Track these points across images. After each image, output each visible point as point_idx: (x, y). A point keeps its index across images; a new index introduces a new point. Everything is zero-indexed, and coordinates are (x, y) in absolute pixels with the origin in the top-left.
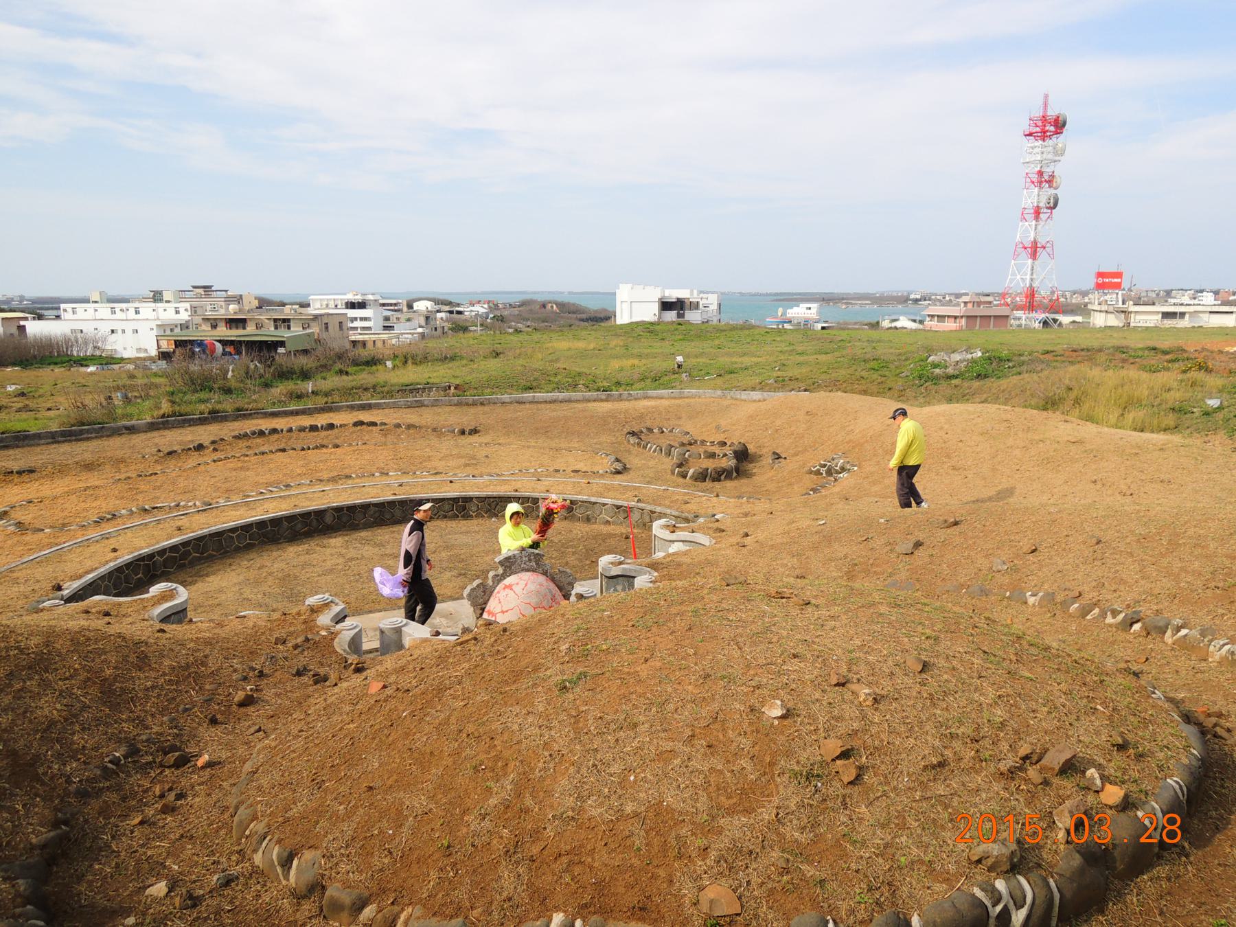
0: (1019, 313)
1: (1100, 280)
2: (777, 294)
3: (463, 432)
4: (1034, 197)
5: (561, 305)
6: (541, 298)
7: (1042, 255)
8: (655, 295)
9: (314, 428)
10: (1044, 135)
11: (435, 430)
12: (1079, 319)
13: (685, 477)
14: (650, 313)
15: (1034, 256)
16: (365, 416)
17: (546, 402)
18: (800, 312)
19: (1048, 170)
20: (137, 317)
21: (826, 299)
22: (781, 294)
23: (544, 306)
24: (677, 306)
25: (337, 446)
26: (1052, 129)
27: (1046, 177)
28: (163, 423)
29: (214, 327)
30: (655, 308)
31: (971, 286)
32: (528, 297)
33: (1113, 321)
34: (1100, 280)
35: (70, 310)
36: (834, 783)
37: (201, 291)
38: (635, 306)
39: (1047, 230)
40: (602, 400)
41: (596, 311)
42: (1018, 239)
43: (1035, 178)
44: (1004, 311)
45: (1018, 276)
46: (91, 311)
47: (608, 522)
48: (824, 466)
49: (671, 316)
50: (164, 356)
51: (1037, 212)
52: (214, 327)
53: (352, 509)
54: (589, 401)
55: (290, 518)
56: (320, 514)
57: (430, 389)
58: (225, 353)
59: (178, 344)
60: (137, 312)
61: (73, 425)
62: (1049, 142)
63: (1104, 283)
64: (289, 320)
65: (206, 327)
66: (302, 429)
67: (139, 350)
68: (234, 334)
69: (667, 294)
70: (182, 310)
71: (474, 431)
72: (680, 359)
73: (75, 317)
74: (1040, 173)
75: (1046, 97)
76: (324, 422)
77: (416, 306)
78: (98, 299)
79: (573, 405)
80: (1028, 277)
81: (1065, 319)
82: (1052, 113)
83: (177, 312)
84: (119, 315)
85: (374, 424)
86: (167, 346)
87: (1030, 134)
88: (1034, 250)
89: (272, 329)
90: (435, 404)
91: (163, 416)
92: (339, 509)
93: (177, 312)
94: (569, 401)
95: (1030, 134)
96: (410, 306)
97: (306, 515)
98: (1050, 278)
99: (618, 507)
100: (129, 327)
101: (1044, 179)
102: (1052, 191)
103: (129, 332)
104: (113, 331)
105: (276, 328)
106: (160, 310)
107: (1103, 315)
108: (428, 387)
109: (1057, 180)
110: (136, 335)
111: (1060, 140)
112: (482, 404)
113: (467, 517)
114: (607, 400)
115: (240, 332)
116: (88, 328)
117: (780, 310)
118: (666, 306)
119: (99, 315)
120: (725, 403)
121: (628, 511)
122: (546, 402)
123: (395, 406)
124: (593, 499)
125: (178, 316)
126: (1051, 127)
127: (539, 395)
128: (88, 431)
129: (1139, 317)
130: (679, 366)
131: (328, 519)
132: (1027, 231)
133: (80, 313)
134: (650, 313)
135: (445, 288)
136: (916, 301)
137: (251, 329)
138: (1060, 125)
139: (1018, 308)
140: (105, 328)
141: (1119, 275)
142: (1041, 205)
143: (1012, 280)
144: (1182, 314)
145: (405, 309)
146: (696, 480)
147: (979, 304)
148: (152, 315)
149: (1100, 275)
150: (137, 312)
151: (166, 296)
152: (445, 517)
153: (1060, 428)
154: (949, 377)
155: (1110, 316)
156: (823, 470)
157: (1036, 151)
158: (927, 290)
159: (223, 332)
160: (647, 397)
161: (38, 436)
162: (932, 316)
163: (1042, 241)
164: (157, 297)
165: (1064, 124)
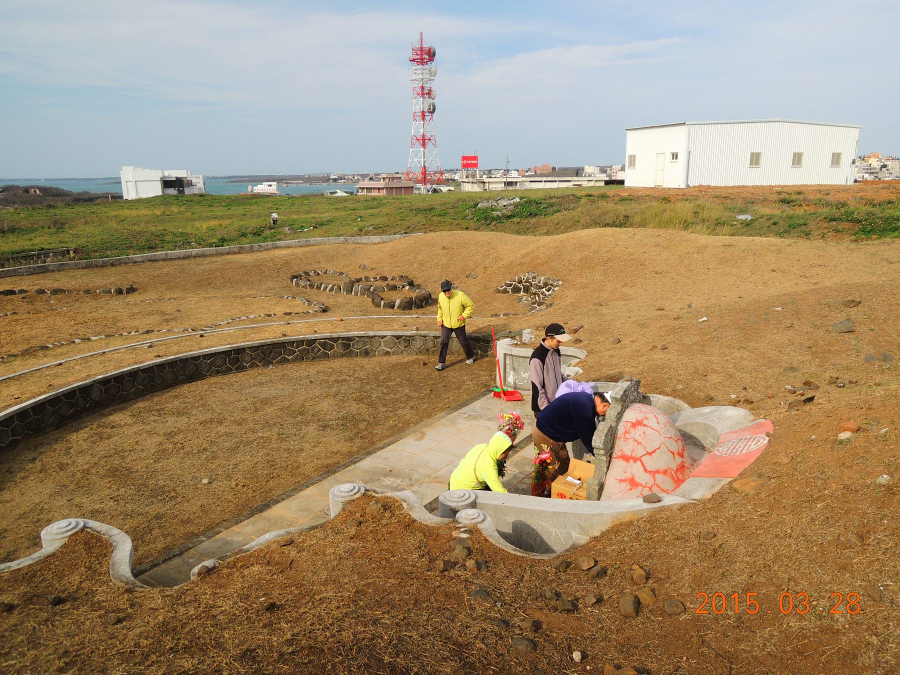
0: (419, 185)
1: (465, 162)
2: (229, 177)
3: (120, 292)
4: (420, 104)
5: (44, 190)
6: (22, 184)
7: (429, 145)
8: (157, 175)
10: (422, 62)
11: (87, 292)
12: (452, 188)
13: (393, 307)
14: (156, 190)
15: (424, 145)
17: (179, 258)
18: (262, 188)
19: (427, 86)
21: (279, 180)
22: (236, 177)
24: (178, 184)
26: (427, 57)
27: (426, 91)
31: (387, 170)
32: (10, 183)
33: (476, 188)
34: (465, 162)
38: (140, 184)
39: (431, 128)
40: (235, 253)
41: (79, 194)
43: (419, 91)
44: (411, 184)
45: (413, 161)
47: (388, 353)
48: (510, 285)
49: (172, 191)
53: (119, 379)
54: (222, 254)
55: (53, 401)
56: (84, 390)
57: (47, 255)
62: (425, 66)
69: (166, 174)
71: (131, 290)
72: (275, 215)
75: (421, 34)
79: (209, 259)
81: (444, 189)
82: (426, 46)
85: (12, 292)
87: (414, 60)
88: (424, 141)
90: (61, 268)
92: (105, 381)
94: (203, 256)
95: (414, 60)
97: (70, 395)
98: (438, 159)
99: (398, 337)
101: (426, 93)
102: (431, 101)
107: (470, 185)
108: (43, 253)
111: (433, 65)
112: (113, 265)
113: (241, 369)
114: (239, 253)
117: (250, 188)
120: (351, 247)
121: (409, 340)
124: (371, 334)
126: (425, 56)
127: (160, 253)
129: (491, 186)
130: (275, 222)
131: (95, 395)
132: (418, 128)
134: (156, 190)
136: (335, 180)
138: (431, 55)
139: (417, 182)
141: (475, 158)
143: (412, 162)
144: (516, 183)
146: (404, 309)
147: (393, 178)
149: (464, 158)
152: (218, 372)
153: (717, 237)
154: (509, 217)
155: (475, 185)
156: (509, 289)
157: (417, 73)
158: (341, 173)
160: (276, 248)
162: (363, 188)
163: (428, 135)
165: (434, 54)
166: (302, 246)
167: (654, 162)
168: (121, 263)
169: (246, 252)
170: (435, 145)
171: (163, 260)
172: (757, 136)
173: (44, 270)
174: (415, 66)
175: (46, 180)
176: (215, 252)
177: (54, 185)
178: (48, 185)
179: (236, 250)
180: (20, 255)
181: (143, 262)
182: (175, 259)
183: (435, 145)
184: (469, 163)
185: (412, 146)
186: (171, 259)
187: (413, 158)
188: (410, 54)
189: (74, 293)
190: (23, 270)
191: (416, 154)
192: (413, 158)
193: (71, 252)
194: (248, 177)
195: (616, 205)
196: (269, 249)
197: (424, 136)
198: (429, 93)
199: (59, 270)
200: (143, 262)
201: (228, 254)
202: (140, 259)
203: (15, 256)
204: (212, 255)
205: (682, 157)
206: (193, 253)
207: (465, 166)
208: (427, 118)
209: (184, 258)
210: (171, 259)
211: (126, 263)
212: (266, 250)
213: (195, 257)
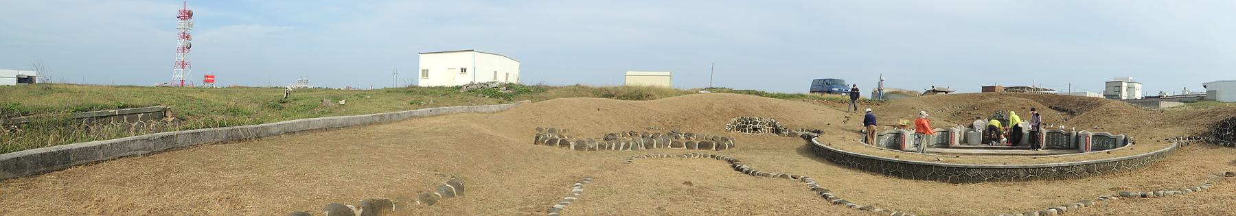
4: (181, 43)
8: (15, 73)
10: (184, 18)
40: (377, 123)
88: (183, 65)
132: (180, 57)
134: (13, 82)
138: (190, 15)
157: (182, 24)
167: (441, 71)
171: (303, 131)
172: (464, 59)
174: (180, 21)
179: (377, 119)
188: (177, 13)
190: (138, 145)
195: (416, 95)
205: (208, 85)
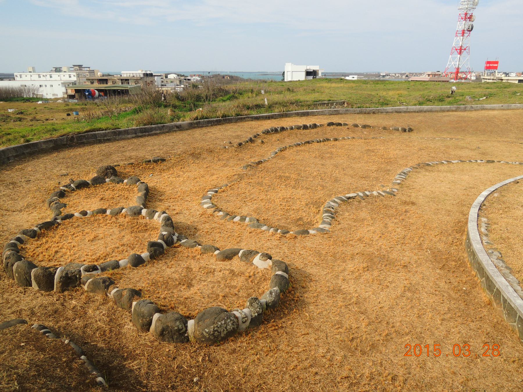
1: (488, 65)
3: (404, 130)
4: (462, 25)
6: (223, 74)
7: (464, 53)
8: (304, 68)
9: (305, 127)
11: (385, 128)
15: (460, 53)
16: (335, 119)
17: (415, 112)
20: (51, 79)
21: (358, 74)
23: (223, 77)
25: (336, 140)
28: (197, 123)
29: (92, 83)
30: (304, 74)
34: (488, 65)
35: (19, 76)
36: (6, 229)
37: (77, 68)
39: (469, 41)
40: (453, 111)
42: (454, 45)
43: (463, 16)
45: (452, 63)
46: (29, 76)
49: (311, 78)
50: (72, 97)
51: (463, 33)
52: (92, 83)
54: (443, 111)
57: (332, 104)
58: (99, 95)
59: (77, 91)
60: (51, 77)
61: (145, 125)
63: (490, 66)
64: (128, 80)
65: (88, 83)
66: (299, 128)
67: (54, 95)
68: (103, 86)
69: (308, 68)
70: (72, 76)
73: (21, 79)
74: (466, 14)
76: (311, 123)
77: (169, 76)
78: (32, 71)
80: (458, 63)
83: (70, 77)
84: (44, 79)
86: (71, 92)
89: (120, 84)
90: (346, 112)
91: (197, 118)
93: (70, 77)
94: (431, 111)
96: (166, 77)
100: (48, 84)
101: (469, 17)
102: (471, 23)
103: (48, 86)
104: (41, 86)
105: (122, 83)
106: (62, 76)
109: (473, 17)
110: (53, 87)
112: (374, 113)
114: (456, 111)
115: (105, 85)
116: (29, 84)
118: (308, 73)
119: (33, 78)
122: (415, 112)
123: (322, 114)
125: (70, 79)
128: (155, 129)
132: (458, 42)
133: (24, 78)
134: (302, 77)
135: (182, 70)
137: (110, 84)
140: (37, 84)
141: (497, 63)
142: (465, 29)
143: (449, 65)
145: (164, 78)
147: (435, 75)
148: (59, 78)
149: (489, 62)
150: (51, 77)
151: (64, 69)
158: (387, 72)
159: (96, 85)
160: (483, 109)
161: (126, 132)
163: (464, 47)
164: (58, 70)
166: (504, 110)
168: (378, 112)
169: (461, 111)
170: (469, 53)
173: (337, 113)
175: (230, 72)
176: (439, 110)
177: (236, 75)
178: (233, 75)
179: (454, 109)
180: (318, 103)
181: (392, 112)
182: (412, 112)
183: (469, 53)
184: (491, 66)
185: (452, 53)
186: (409, 112)
187: (450, 62)
189: (376, 128)
191: (454, 59)
192: (450, 62)
193: (345, 103)
194: (331, 73)
196: (478, 110)
197: (461, 47)
198: (470, 18)
199: (345, 114)
200: (392, 112)
201: (448, 111)
202: (391, 111)
203: (315, 103)
204: (437, 111)
206: (425, 109)
207: (488, 68)
208: (466, 35)
209: (418, 112)
210: (409, 112)
211: (382, 112)
212: (475, 110)
213: (425, 112)
